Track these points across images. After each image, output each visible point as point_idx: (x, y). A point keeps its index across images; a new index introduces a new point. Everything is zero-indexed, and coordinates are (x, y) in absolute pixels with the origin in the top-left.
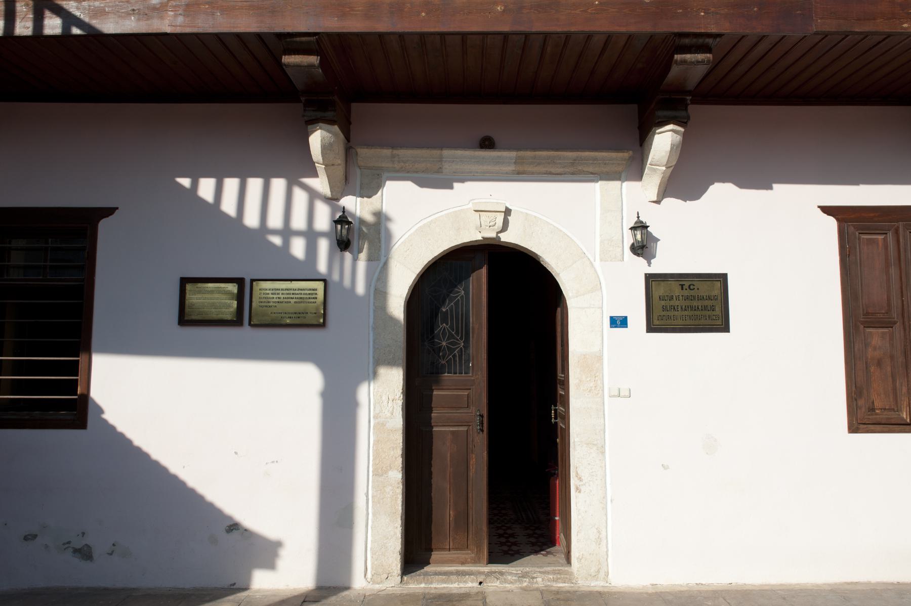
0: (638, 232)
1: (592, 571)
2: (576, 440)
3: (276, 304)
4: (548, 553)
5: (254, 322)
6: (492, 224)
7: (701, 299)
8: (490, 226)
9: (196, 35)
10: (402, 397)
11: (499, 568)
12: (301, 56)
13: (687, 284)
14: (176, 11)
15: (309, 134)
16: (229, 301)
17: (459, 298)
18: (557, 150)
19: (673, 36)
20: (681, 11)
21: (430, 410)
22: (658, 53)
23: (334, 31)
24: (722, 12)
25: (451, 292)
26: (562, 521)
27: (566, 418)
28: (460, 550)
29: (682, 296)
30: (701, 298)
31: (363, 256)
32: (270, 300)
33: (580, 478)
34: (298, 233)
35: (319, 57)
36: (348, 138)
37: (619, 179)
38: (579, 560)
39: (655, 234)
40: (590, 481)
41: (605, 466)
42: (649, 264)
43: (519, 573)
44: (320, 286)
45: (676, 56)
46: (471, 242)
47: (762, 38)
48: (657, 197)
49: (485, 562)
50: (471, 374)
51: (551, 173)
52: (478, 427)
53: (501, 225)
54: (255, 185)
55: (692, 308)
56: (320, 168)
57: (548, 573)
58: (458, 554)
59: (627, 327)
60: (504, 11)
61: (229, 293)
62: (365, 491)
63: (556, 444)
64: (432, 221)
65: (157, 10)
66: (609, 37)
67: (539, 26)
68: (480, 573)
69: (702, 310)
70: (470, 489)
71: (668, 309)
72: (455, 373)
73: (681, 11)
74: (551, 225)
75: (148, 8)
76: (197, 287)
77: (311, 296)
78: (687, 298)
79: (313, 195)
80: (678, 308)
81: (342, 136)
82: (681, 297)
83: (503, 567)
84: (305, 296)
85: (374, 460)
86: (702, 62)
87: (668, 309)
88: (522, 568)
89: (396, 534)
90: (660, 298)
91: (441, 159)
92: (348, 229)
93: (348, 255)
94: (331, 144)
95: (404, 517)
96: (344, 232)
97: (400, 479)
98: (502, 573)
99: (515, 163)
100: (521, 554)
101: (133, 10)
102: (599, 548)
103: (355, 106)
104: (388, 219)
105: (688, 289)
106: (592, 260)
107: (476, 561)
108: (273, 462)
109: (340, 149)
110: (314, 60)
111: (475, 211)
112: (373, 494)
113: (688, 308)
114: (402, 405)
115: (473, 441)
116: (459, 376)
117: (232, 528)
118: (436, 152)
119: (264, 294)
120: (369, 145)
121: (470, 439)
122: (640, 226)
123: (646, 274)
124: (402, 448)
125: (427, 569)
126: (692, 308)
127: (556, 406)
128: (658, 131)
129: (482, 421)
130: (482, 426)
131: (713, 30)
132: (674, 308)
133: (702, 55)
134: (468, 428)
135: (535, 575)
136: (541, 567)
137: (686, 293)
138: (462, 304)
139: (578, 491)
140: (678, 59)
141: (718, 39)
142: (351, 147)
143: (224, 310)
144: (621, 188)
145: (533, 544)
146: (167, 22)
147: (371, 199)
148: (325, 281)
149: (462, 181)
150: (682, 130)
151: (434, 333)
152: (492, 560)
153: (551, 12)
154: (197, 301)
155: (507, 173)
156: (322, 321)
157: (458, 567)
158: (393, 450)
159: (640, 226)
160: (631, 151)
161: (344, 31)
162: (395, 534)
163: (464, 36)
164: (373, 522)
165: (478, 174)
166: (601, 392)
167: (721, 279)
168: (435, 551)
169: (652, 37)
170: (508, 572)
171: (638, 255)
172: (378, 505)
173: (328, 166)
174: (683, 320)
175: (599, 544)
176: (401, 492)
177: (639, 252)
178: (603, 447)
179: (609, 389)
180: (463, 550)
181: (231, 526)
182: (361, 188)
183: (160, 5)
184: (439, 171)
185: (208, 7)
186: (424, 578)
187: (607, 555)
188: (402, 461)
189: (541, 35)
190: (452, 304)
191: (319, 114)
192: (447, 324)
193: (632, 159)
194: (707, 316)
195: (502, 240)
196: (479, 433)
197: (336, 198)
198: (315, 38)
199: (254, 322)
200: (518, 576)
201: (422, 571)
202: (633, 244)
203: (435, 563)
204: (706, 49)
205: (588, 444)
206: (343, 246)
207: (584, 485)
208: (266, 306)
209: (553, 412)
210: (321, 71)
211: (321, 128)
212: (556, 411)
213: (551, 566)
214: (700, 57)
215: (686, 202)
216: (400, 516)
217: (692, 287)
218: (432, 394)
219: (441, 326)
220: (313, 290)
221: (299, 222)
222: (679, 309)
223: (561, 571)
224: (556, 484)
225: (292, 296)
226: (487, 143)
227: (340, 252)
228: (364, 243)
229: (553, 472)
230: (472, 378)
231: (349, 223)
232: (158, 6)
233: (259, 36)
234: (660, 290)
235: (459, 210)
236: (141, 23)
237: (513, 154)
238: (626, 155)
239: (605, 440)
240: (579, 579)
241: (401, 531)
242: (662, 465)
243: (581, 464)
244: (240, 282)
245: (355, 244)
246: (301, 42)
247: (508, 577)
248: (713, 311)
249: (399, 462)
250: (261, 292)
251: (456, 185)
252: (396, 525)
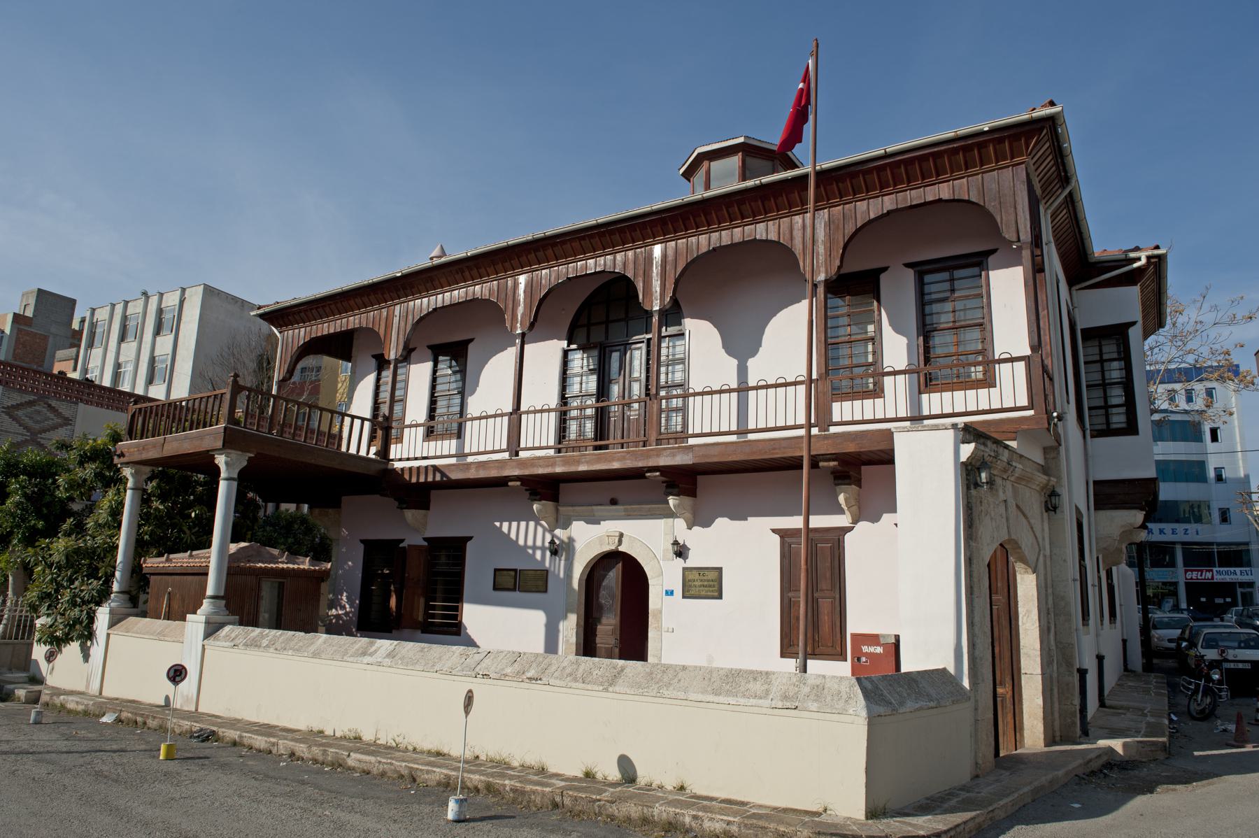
13: (702, 573)
31: (563, 558)
34: (539, 548)
42: (685, 562)
79: (545, 530)
122: (676, 543)
126: (704, 586)
137: (702, 578)
149: (604, 520)
221: (539, 543)
251: (602, 522)
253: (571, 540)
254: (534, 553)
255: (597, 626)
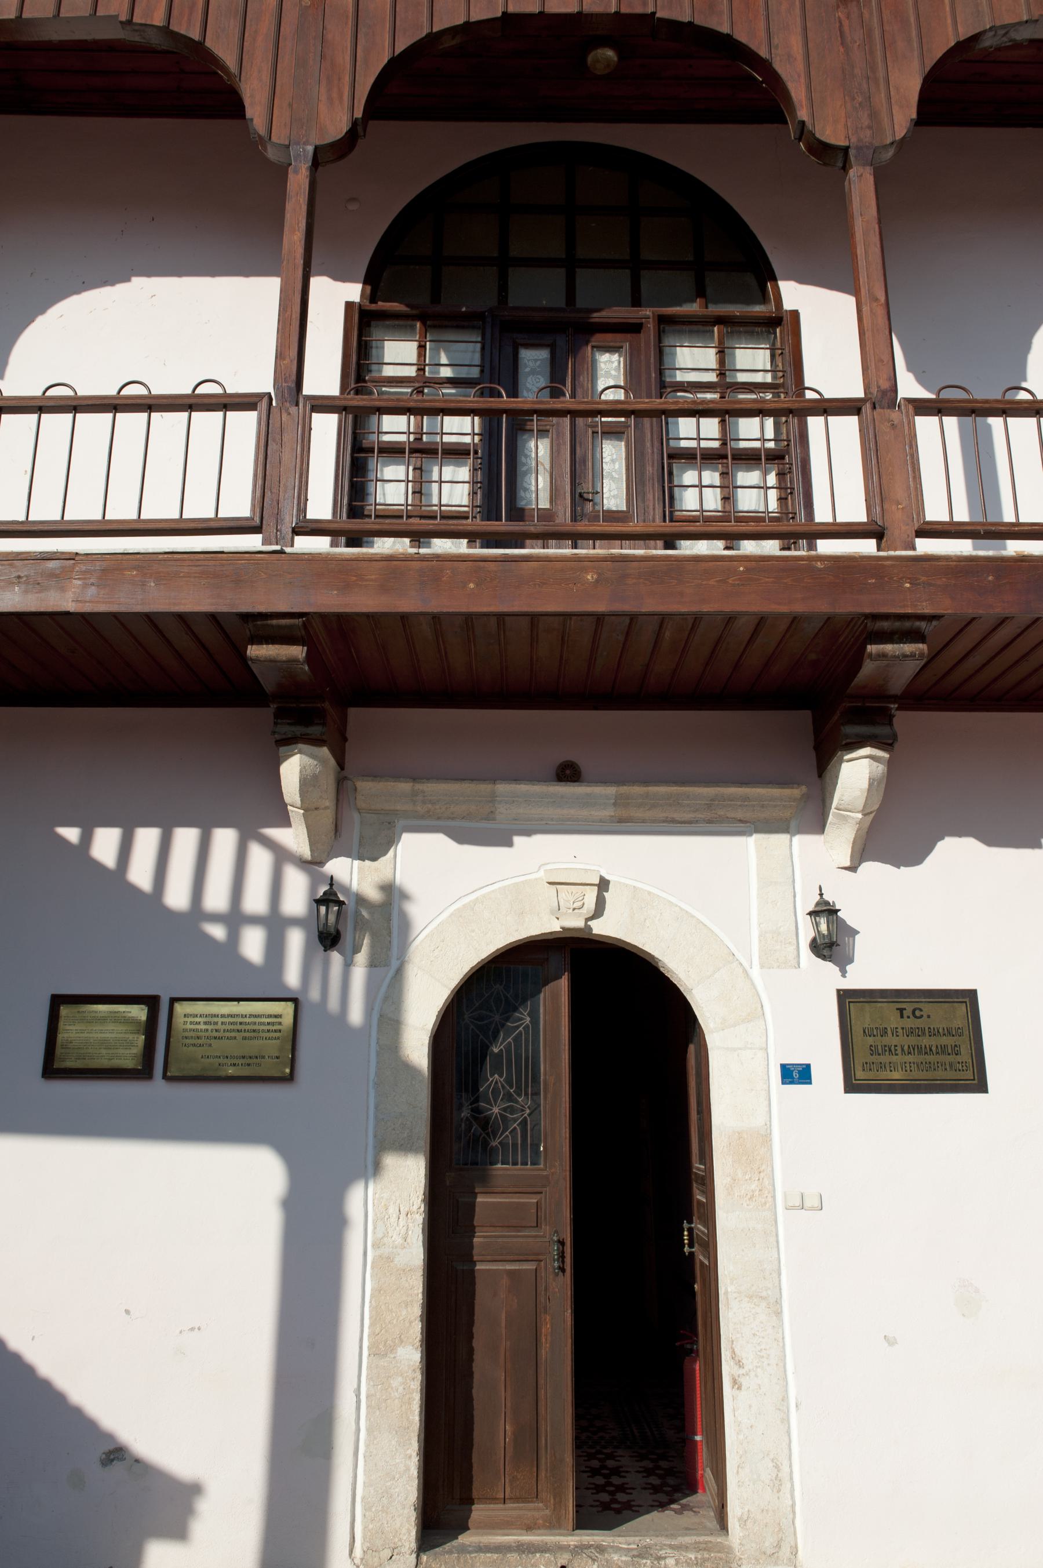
0: (822, 919)
1: (767, 1544)
2: (729, 1290)
3: (212, 1041)
4: (685, 1508)
5: (172, 1072)
6: (577, 905)
7: (935, 1035)
8: (574, 909)
9: (115, 616)
10: (422, 1209)
11: (596, 1538)
12: (277, 646)
13: (909, 1008)
14: (85, 579)
15: (281, 759)
16: (131, 1037)
17: (521, 1029)
18: (683, 783)
19: (863, 618)
20: (874, 581)
21: (471, 1231)
22: (841, 640)
23: (332, 611)
24: (939, 582)
25: (507, 1019)
26: (707, 1442)
27: (710, 1245)
28: (523, 1502)
29: (903, 1028)
30: (934, 1033)
31: (361, 958)
32: (200, 1034)
33: (739, 1361)
34: (254, 920)
35: (305, 648)
36: (341, 765)
37: (785, 830)
38: (743, 1522)
39: (850, 922)
40: (757, 1367)
41: (783, 1338)
42: (844, 973)
43: (632, 1549)
44: (286, 1010)
45: (869, 647)
46: (542, 934)
47: (1003, 621)
48: (851, 860)
49: (571, 1528)
50: (542, 1166)
51: (673, 821)
52: (556, 1264)
53: (593, 906)
54: (186, 838)
55: (920, 1050)
56: (296, 814)
57: (686, 1548)
58: (520, 1509)
59: (810, 1083)
60: (597, 581)
61: (133, 1021)
62: (356, 1386)
63: (693, 1294)
64: (477, 898)
65: (56, 577)
66: (762, 621)
67: (651, 605)
68: (561, 1548)
69: (937, 1053)
70: (541, 1382)
71: (880, 1051)
72: (515, 1163)
73: (874, 581)
74: (677, 906)
75: (41, 574)
76: (79, 1012)
77: (270, 1027)
78: (911, 1032)
79: (281, 856)
80: (896, 1050)
81: (332, 762)
82: (900, 1030)
83: (604, 1535)
84: (262, 1027)
85: (371, 1325)
86: (912, 655)
87: (880, 1051)
88: (637, 1539)
89: (409, 1470)
90: (864, 1032)
91: (492, 798)
92: (339, 913)
93: (336, 958)
94: (315, 777)
95: (423, 1436)
96: (332, 918)
97: (418, 1364)
98: (601, 1549)
99: (615, 804)
100: (628, 1491)
101: (19, 577)
102: (778, 1498)
103: (353, 712)
104: (404, 896)
105: (911, 1016)
106: (746, 965)
107: (553, 1524)
108: (192, 1329)
109: (329, 783)
110: (298, 652)
111: (550, 883)
112: (368, 1390)
113: (914, 1049)
114: (423, 1224)
115: (546, 1290)
116: (520, 1170)
117: (112, 1457)
118: (485, 788)
119: (191, 1023)
120: (375, 775)
121: (541, 1288)
122: (825, 910)
123: (838, 991)
124: (422, 1304)
125: (465, 1539)
126: (920, 1050)
127: (690, 1222)
128: (846, 757)
129: (563, 1252)
130: (563, 1262)
131: (927, 609)
132: (889, 1050)
133: (910, 645)
134: (538, 1265)
135: (662, 1553)
136: (673, 1536)
137: (910, 1023)
138: (527, 1040)
139: (737, 1386)
140: (874, 652)
141: (934, 623)
142: (345, 778)
143: (121, 1051)
144: (791, 845)
145: (656, 1489)
146: (70, 595)
147: (376, 863)
148: (295, 1001)
149: (528, 833)
150: (886, 755)
151: (479, 1090)
152: (582, 1523)
153: (672, 583)
154: (77, 1035)
155: (601, 821)
156: (288, 1071)
157: (521, 1535)
158: (406, 1306)
159: (825, 910)
160: (804, 787)
161: (348, 610)
162: (408, 1469)
163: (534, 618)
164: (367, 1446)
165: (554, 822)
166: (770, 1199)
167: (967, 1000)
168: (477, 1504)
169: (829, 619)
170: (612, 1547)
171: (824, 958)
172: (378, 1413)
173: (309, 810)
174: (906, 1071)
175: (779, 1491)
176: (419, 1388)
177: (826, 952)
178: (778, 1302)
179: (785, 1195)
180: (529, 1502)
181: (111, 1452)
182: (361, 844)
183: (61, 570)
184: (490, 816)
185: (137, 574)
186: (458, 1559)
187: (794, 1512)
188: (422, 1328)
189: (656, 617)
190: (509, 1039)
191: (299, 730)
192: (501, 1076)
193: (806, 798)
194: (947, 1064)
195: (594, 932)
196: (557, 1275)
197: (318, 861)
198: (300, 620)
199: (172, 1072)
200: (631, 1554)
201: (455, 1543)
202: (814, 940)
203: (478, 1528)
204: (917, 636)
205: (751, 1297)
206: (328, 943)
207: (747, 1374)
208: (194, 1045)
209: (686, 1233)
210: (307, 668)
211: (300, 752)
212: (691, 1231)
213: (691, 1535)
214: (908, 648)
215: (899, 868)
216: (416, 1434)
217: (918, 1013)
218: (475, 1202)
219: (491, 1079)
220: (276, 1016)
221: (256, 901)
222: (899, 1051)
223: (710, 1545)
224: (694, 1370)
225: (239, 1027)
226: (568, 772)
227: (323, 952)
228: (364, 936)
229: (688, 1346)
230: (545, 1173)
231: (341, 903)
232: (58, 572)
233: (213, 617)
234: (863, 1017)
235: (522, 882)
236: (30, 596)
237: (611, 790)
238: (796, 792)
239: (780, 1289)
240: (744, 1562)
241: (417, 1463)
242: (885, 1336)
243: (739, 1335)
244: (151, 1002)
245: (347, 938)
246: (280, 627)
247: (613, 1555)
248: (957, 1054)
249: (416, 1330)
250: (186, 1019)
251: (517, 840)
252: (409, 1452)
253: (393, 894)
254: (234, 937)
255: (475, 1195)
